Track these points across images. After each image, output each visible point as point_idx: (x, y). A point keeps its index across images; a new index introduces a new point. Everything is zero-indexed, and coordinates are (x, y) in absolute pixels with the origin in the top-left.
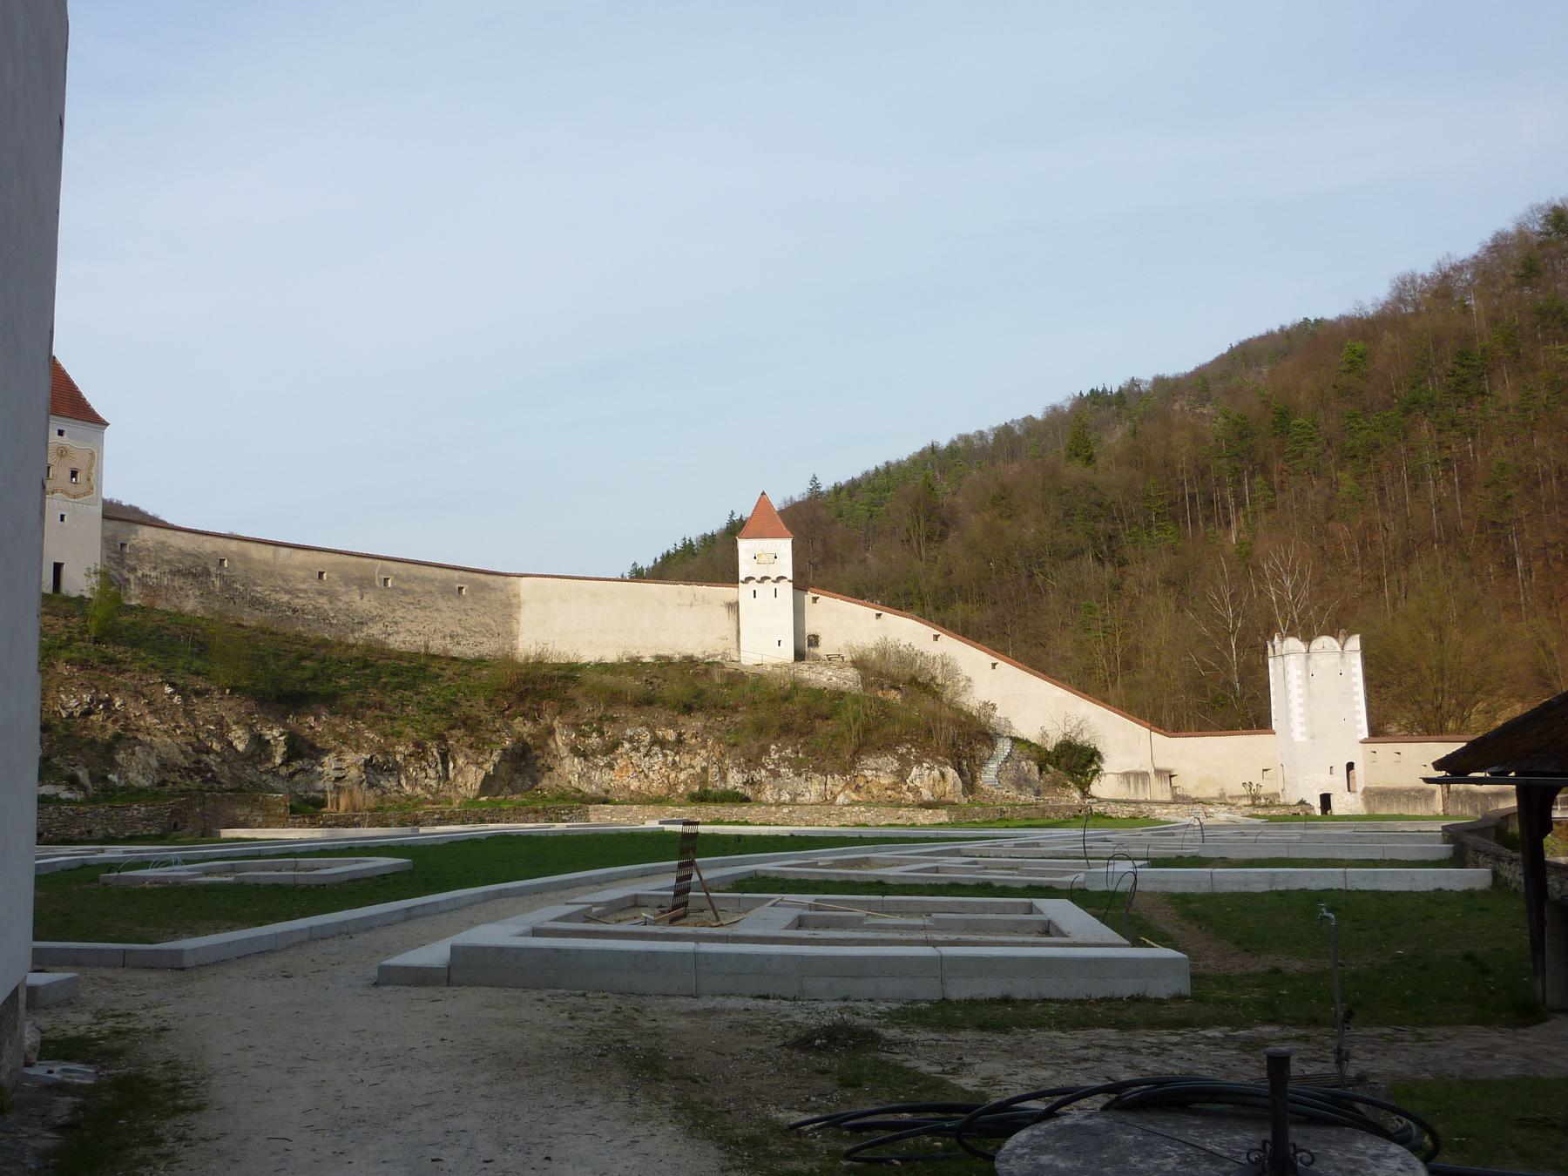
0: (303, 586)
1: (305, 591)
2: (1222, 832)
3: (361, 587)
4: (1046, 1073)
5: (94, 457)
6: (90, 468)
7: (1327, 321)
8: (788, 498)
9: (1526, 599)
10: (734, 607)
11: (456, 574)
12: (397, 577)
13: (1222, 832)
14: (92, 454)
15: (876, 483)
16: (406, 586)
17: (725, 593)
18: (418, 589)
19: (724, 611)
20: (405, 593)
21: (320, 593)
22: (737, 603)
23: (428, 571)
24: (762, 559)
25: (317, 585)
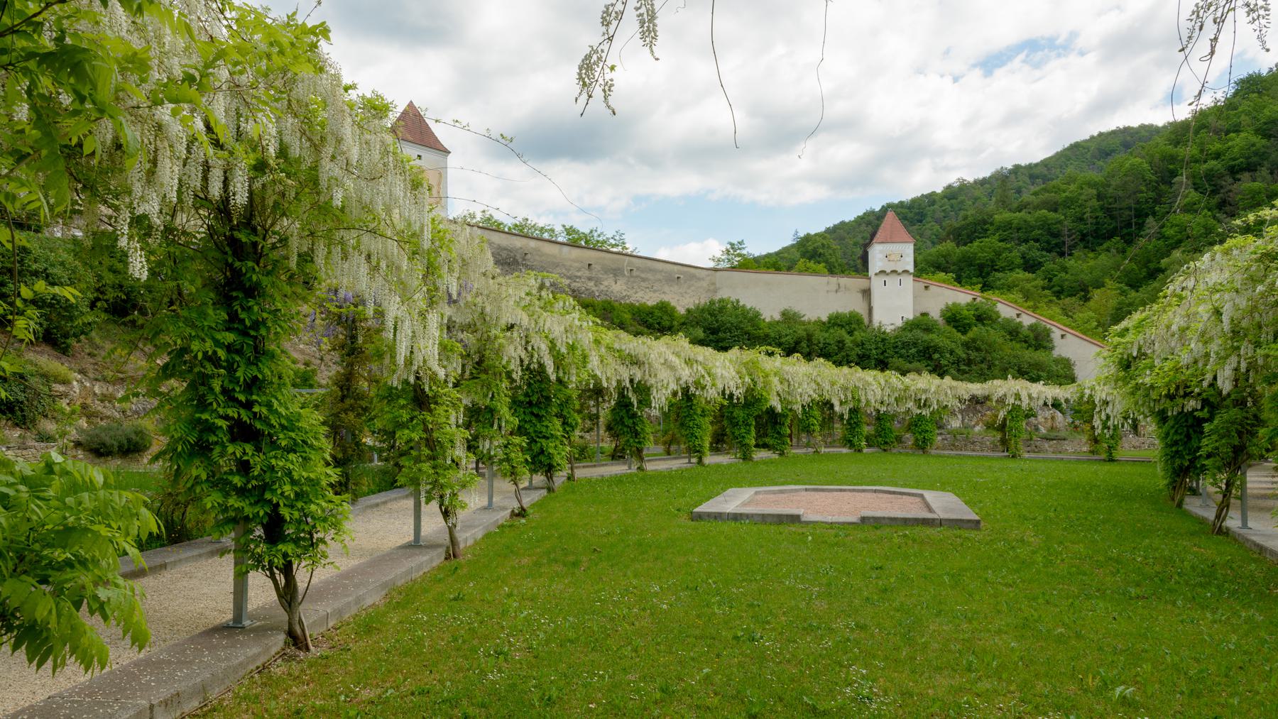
0: (579, 274)
1: (580, 277)
2: (1256, 479)
3: (615, 275)
4: (736, 500)
5: (441, 173)
6: (439, 184)
7: (1133, 128)
8: (999, 167)
9: (430, 387)
10: (867, 293)
11: (676, 267)
12: (638, 269)
13: (1256, 479)
14: (440, 174)
15: (1036, 171)
16: (643, 275)
17: (859, 283)
18: (651, 277)
19: (860, 295)
20: (644, 280)
21: (590, 279)
22: (869, 290)
23: (660, 266)
24: (891, 258)
25: (587, 273)
